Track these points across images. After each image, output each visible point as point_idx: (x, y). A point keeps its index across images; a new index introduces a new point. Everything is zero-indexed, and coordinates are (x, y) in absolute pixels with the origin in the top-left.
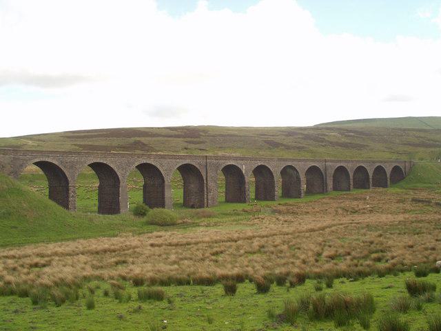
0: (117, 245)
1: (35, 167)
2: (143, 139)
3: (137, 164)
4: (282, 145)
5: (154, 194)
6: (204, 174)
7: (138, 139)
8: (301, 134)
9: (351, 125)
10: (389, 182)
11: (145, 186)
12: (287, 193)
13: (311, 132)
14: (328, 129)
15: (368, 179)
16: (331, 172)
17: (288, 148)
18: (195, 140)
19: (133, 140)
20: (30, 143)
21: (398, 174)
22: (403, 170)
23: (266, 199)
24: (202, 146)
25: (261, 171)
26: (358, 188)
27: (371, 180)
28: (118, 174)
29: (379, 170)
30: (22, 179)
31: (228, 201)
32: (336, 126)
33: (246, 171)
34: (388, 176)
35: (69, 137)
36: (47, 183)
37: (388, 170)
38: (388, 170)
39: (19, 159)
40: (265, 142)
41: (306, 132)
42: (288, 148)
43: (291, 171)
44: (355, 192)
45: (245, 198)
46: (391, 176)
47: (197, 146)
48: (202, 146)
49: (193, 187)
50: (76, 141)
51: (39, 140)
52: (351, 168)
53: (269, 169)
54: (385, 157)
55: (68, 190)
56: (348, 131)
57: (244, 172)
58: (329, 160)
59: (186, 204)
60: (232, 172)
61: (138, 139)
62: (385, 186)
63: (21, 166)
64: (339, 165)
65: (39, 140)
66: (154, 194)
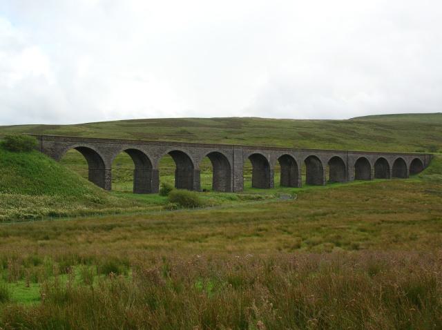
0: (76, 233)
1: (75, 151)
2: (188, 129)
3: (169, 151)
4: (314, 136)
5: (186, 176)
6: (230, 161)
7: (184, 128)
8: (334, 127)
9: (376, 120)
10: (408, 173)
11: (177, 172)
12: (311, 181)
13: (343, 125)
14: (359, 122)
15: (389, 172)
16: (352, 163)
17: (320, 139)
18: (237, 130)
19: (179, 129)
20: (88, 130)
21: (418, 165)
22: (423, 163)
23: (290, 186)
24: (242, 136)
25: (286, 161)
26: (378, 178)
27: (391, 171)
28: (150, 159)
29: (399, 162)
30: (65, 162)
31: (254, 186)
32: (370, 120)
33: (271, 160)
34: (408, 168)
35: (123, 126)
36: (87, 166)
37: (408, 162)
38: (408, 162)
39: (59, 144)
40: (299, 133)
41: (338, 125)
42: (320, 139)
43: (313, 160)
44: (375, 181)
45: (269, 185)
46: (411, 167)
47: (237, 136)
48: (242, 136)
49: (222, 173)
50: (350, 127)
51: (97, 128)
52: (372, 160)
53: (293, 159)
54: (402, 148)
55: (104, 173)
56: (378, 124)
57: (269, 161)
58: (371, 150)
59: (216, 187)
60: (259, 160)
61: (184, 128)
62: (406, 177)
63: (62, 150)
64: (360, 156)
65: (97, 128)
66: (186, 176)
